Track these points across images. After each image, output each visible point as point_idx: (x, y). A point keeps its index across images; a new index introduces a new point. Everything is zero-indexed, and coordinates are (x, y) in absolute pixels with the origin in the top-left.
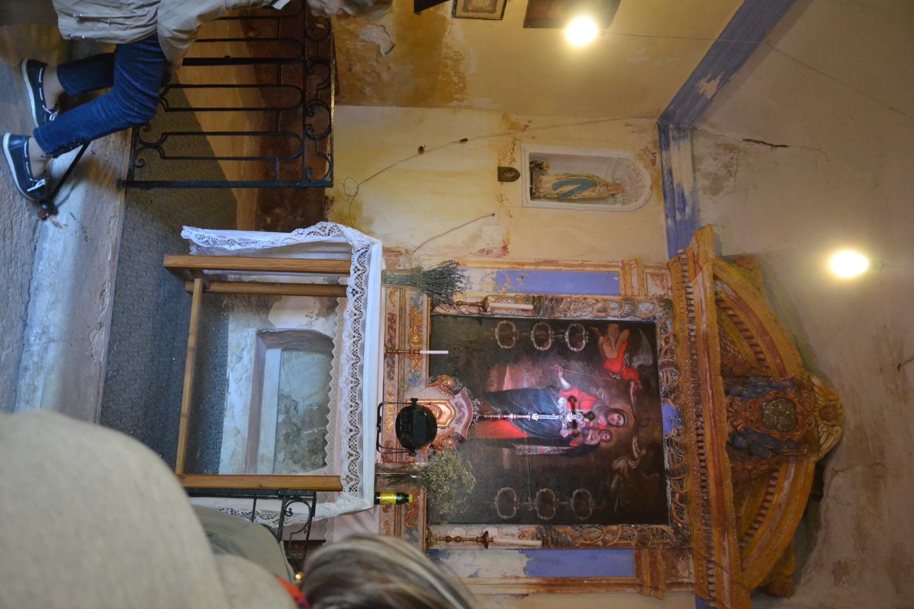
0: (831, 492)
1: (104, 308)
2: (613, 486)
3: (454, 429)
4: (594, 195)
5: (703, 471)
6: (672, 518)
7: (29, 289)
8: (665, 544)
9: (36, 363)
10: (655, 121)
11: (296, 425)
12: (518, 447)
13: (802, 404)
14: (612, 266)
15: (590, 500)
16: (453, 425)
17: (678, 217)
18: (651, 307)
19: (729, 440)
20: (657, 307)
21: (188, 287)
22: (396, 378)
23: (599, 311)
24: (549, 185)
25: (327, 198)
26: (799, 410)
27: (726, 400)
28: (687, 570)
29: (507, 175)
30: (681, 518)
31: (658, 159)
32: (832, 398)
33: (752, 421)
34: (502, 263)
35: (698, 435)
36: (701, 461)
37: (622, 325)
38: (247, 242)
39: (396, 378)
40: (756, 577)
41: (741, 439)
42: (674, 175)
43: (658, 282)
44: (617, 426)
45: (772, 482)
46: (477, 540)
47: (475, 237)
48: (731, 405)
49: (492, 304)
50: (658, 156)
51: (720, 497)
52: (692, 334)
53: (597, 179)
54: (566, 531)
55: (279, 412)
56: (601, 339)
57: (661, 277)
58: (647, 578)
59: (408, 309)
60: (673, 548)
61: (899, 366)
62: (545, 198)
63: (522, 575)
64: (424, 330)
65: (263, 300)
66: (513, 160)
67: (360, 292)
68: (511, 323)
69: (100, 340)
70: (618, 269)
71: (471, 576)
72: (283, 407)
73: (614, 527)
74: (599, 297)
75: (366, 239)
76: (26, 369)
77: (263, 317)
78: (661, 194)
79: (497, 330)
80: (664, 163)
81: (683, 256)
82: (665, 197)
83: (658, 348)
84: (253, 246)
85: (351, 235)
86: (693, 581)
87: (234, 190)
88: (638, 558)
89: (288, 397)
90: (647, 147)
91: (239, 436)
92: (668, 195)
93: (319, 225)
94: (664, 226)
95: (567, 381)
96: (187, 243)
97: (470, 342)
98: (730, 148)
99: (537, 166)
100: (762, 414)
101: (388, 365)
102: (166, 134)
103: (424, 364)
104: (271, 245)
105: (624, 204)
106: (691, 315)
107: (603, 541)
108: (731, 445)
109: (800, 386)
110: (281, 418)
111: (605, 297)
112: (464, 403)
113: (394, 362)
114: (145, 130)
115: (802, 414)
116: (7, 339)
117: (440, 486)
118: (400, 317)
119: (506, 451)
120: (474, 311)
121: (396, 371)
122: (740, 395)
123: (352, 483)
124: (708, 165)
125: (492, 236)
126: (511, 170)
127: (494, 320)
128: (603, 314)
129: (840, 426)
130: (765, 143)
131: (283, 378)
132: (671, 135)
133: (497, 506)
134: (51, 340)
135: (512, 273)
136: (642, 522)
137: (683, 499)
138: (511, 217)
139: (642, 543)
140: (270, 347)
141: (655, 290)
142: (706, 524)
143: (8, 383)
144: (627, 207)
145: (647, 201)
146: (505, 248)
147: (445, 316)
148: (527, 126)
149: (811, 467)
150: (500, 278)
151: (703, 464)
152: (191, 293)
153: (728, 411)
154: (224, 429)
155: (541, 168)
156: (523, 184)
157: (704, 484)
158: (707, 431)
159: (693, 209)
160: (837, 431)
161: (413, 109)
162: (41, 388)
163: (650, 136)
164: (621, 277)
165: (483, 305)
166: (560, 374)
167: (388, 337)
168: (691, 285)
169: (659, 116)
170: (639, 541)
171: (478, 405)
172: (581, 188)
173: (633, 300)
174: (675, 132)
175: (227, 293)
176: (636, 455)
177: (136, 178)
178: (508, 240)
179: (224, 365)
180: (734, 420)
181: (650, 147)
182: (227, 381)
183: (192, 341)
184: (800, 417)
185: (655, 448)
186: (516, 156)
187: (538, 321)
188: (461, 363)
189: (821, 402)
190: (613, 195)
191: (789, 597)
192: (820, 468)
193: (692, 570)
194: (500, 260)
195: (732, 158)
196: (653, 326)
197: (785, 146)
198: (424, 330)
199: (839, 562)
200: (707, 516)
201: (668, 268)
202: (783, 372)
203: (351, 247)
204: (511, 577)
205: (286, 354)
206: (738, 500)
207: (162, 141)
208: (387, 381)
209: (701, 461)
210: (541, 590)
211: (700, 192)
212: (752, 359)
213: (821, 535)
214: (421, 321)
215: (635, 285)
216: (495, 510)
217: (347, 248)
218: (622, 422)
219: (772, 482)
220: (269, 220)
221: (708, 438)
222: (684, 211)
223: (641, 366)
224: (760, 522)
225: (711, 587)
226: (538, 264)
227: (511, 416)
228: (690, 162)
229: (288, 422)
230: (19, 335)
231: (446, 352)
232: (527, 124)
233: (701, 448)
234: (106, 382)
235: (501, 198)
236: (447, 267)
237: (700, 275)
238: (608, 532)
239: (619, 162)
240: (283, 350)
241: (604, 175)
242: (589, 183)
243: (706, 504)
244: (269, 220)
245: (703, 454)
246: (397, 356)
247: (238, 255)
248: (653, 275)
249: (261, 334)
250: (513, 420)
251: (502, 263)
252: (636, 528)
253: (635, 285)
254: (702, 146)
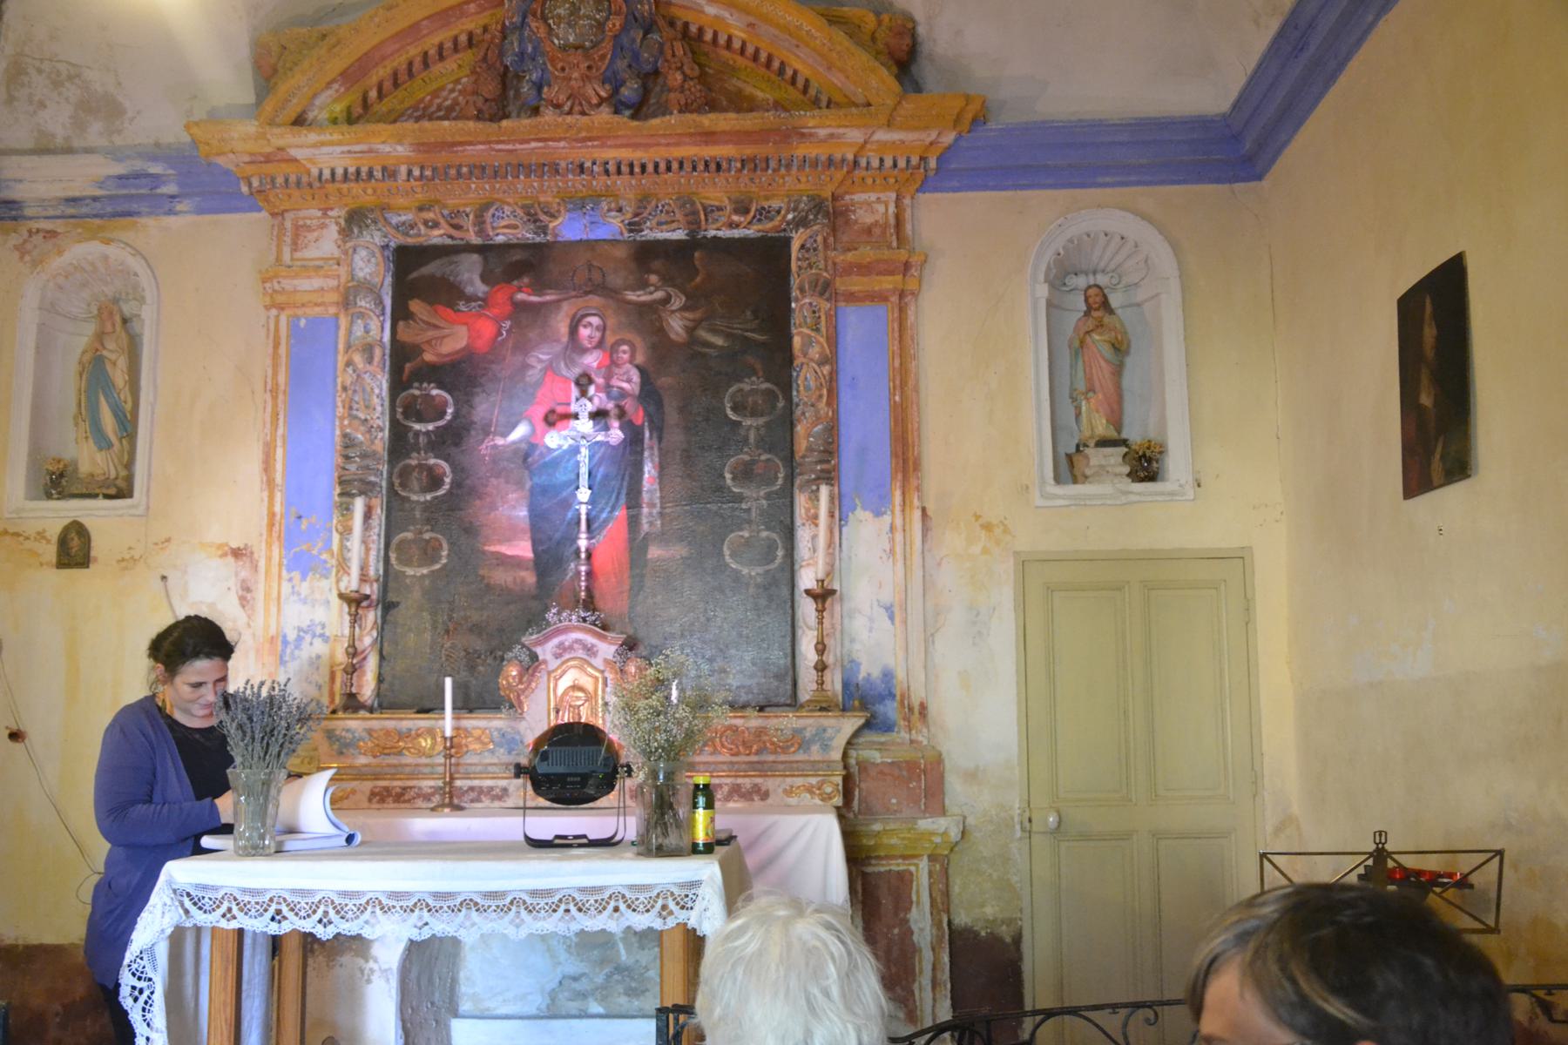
3: (606, 661)
12: (645, 527)
16: (598, 662)
101: (478, 800)
112: (556, 641)
113: (472, 789)
119: (654, 552)
171: (559, 613)
188: (478, 644)
227: (583, 543)
250: (589, 539)
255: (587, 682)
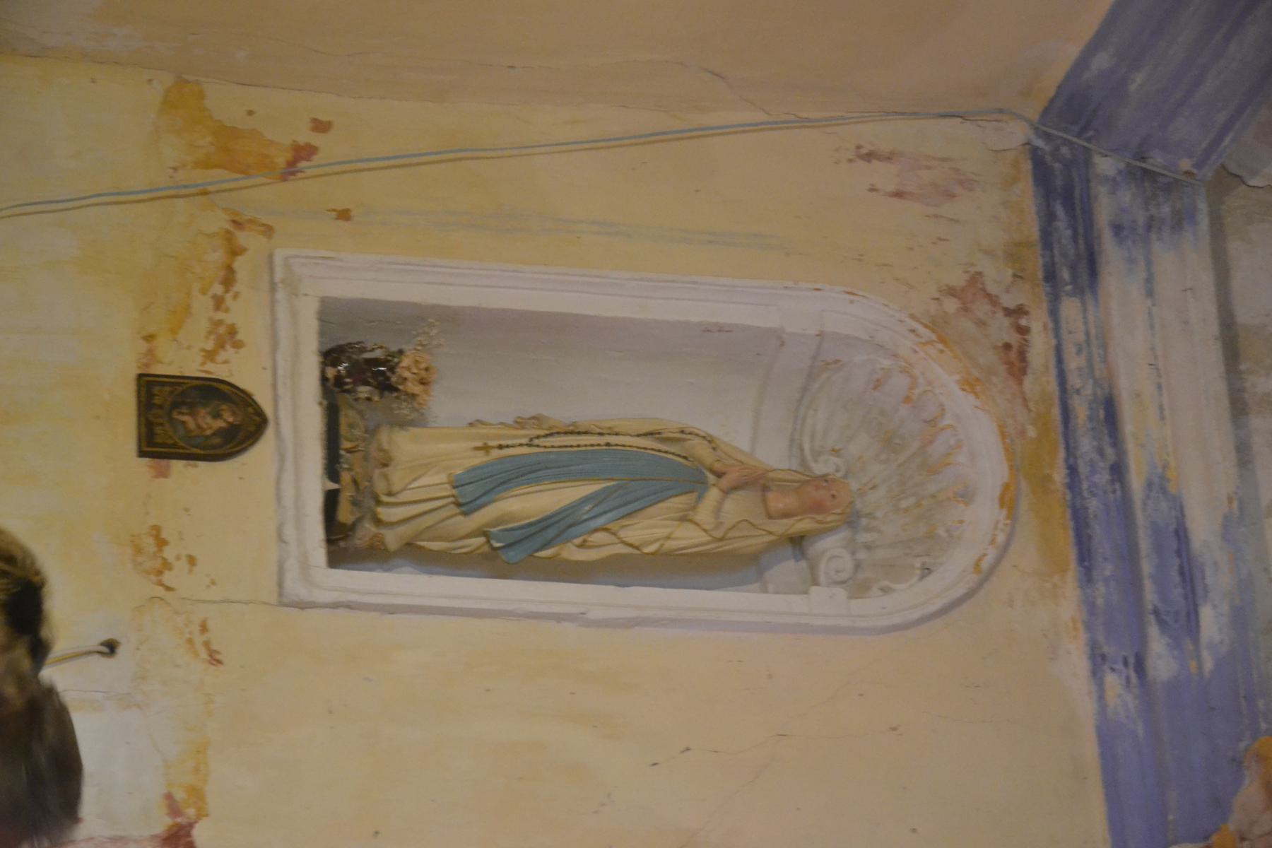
4: (687, 537)
10: (1017, 134)
24: (435, 482)
31: (1040, 347)
42: (1129, 427)
50: (1037, 323)
53: (702, 451)
62: (416, 554)
66: (228, 337)
80: (1074, 363)
82: (1085, 555)
90: (975, 279)
92: (1103, 544)
94: (1086, 708)
99: (363, 374)
105: (858, 588)
126: (212, 392)
132: (1105, 209)
138: (215, 659)
144: (872, 609)
145: (985, 575)
148: (303, 153)
155: (386, 387)
156: (288, 468)
163: (996, 218)
169: (1033, 111)
174: (1126, 196)
178: (197, 794)
181: (996, 275)
186: (246, 312)
190: (798, 542)
228: (1213, 356)
232: (305, 136)
239: (822, 362)
241: (744, 428)
242: (670, 469)
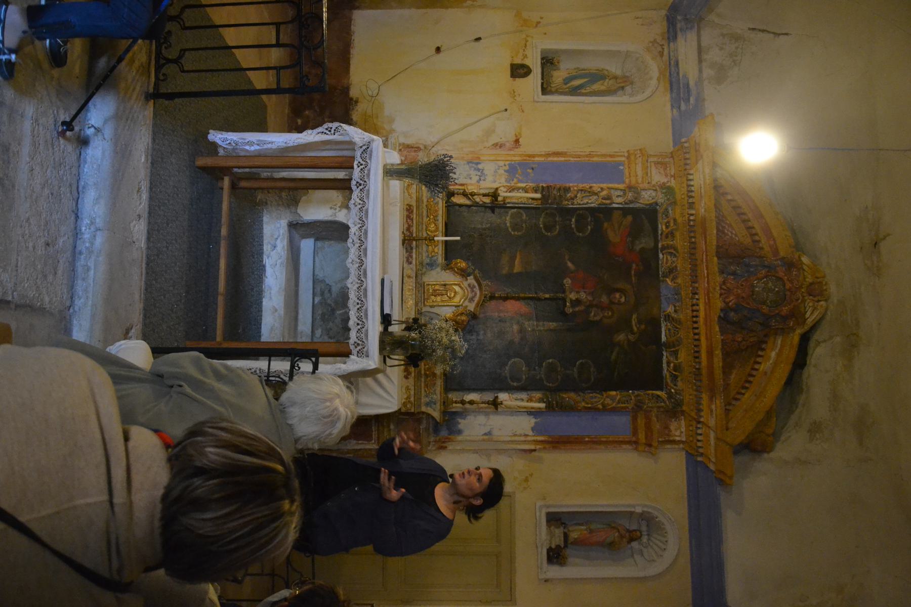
0: (813, 361)
1: (141, 203)
2: (613, 357)
4: (603, 88)
5: (696, 343)
6: (667, 384)
7: (78, 187)
8: (659, 407)
9: (87, 248)
11: (330, 305)
13: (791, 281)
14: (618, 156)
15: (592, 369)
16: (467, 303)
17: (683, 107)
18: (654, 194)
19: (722, 315)
20: (659, 193)
21: (220, 184)
22: (414, 262)
23: (604, 199)
24: (560, 80)
25: (351, 99)
26: (787, 287)
27: (719, 279)
28: (679, 429)
29: (519, 71)
30: (675, 385)
32: (818, 275)
33: (743, 298)
34: (514, 155)
35: (693, 311)
36: (695, 334)
37: (625, 211)
38: (265, 143)
39: (414, 262)
40: (739, 437)
41: (732, 314)
43: (662, 171)
44: (619, 303)
45: (760, 353)
46: (488, 403)
47: (489, 132)
48: (724, 283)
49: (503, 193)
51: (711, 367)
52: (692, 218)
53: (606, 73)
54: (570, 397)
55: (314, 295)
56: (606, 225)
57: (664, 165)
58: (642, 436)
59: (425, 200)
60: (667, 411)
61: (876, 244)
63: (531, 433)
64: (440, 218)
65: (293, 193)
67: (363, 184)
68: (521, 211)
69: (139, 229)
70: (623, 159)
71: (485, 434)
72: (318, 290)
73: (614, 393)
74: (604, 186)
75: (367, 136)
76: (81, 253)
77: (293, 210)
78: (668, 85)
79: (508, 218)
80: (672, 54)
81: (686, 145)
83: (660, 232)
84: (269, 146)
85: (355, 134)
86: (684, 439)
87: (264, 97)
88: (635, 419)
89: (323, 281)
91: (276, 314)
93: (325, 126)
95: (573, 263)
96: (214, 146)
97: (484, 229)
98: (736, 38)
100: (753, 292)
102: (184, 51)
103: (440, 250)
104: (284, 145)
106: (691, 200)
107: (603, 404)
108: (724, 320)
109: (791, 265)
110: (317, 300)
111: (610, 185)
112: (476, 284)
114: (166, 48)
115: (790, 290)
116: (63, 229)
117: (434, 351)
118: (418, 207)
120: (487, 200)
121: (414, 256)
122: (734, 274)
123: (359, 348)
124: (714, 55)
125: (505, 130)
126: (523, 66)
127: (504, 207)
128: (608, 202)
129: (826, 300)
130: (769, 32)
131: (317, 264)
132: (679, 26)
133: (508, 375)
134: (98, 229)
135: (523, 165)
136: (638, 389)
137: (677, 368)
139: (638, 407)
140: (304, 237)
141: (658, 177)
142: (696, 391)
143: (67, 264)
144: (632, 99)
146: (517, 141)
147: (461, 206)
148: (539, 23)
149: (796, 339)
150: (512, 170)
151: (697, 337)
152: (222, 189)
153: (721, 288)
154: (264, 309)
155: (552, 63)
156: (534, 80)
157: (697, 355)
158: (702, 307)
159: (697, 100)
160: (822, 306)
161: (429, 10)
162: (93, 267)
163: (659, 28)
164: (626, 166)
165: (495, 195)
166: (567, 257)
167: (406, 226)
168: (691, 172)
170: (636, 405)
172: (589, 82)
173: (636, 188)
175: (260, 186)
176: (635, 329)
177: (163, 90)
178: (520, 134)
179: (260, 253)
180: (726, 297)
181: (659, 39)
182: (264, 266)
183: (224, 231)
184: (788, 293)
185: (654, 324)
186: (529, 52)
187: (546, 209)
189: (809, 279)
191: (768, 452)
192: (805, 339)
193: (683, 430)
194: (512, 152)
195: (737, 48)
196: (655, 212)
197: (787, 34)
198: (440, 218)
199: (815, 423)
200: (698, 383)
201: (672, 157)
202: (776, 252)
203: (354, 144)
204: (520, 435)
205: (319, 244)
206: (727, 369)
207: (180, 57)
208: (405, 265)
209: (695, 334)
210: (547, 446)
211: (706, 83)
212: (748, 241)
213: (802, 399)
214: (436, 211)
215: (640, 173)
216: (506, 378)
217: (350, 144)
218: (623, 300)
219: (760, 353)
220: (299, 121)
221: (702, 314)
222: (689, 100)
223: (643, 249)
224: (747, 388)
225: (699, 444)
226: (548, 155)
229: (323, 303)
230: (72, 226)
231: (458, 238)
233: (696, 322)
234: (147, 264)
235: (513, 94)
236: (442, 160)
237: (700, 162)
238: (607, 397)
239: (628, 54)
240: (317, 239)
241: (614, 68)
242: (597, 76)
243: (698, 373)
244: (299, 121)
245: (697, 328)
246: (414, 243)
247: (259, 155)
248: (657, 163)
249: (292, 226)
251: (514, 155)
252: (633, 393)
253: (640, 173)
254: (708, 36)
255: (457, 300)
